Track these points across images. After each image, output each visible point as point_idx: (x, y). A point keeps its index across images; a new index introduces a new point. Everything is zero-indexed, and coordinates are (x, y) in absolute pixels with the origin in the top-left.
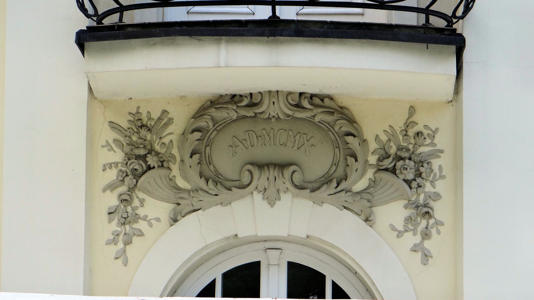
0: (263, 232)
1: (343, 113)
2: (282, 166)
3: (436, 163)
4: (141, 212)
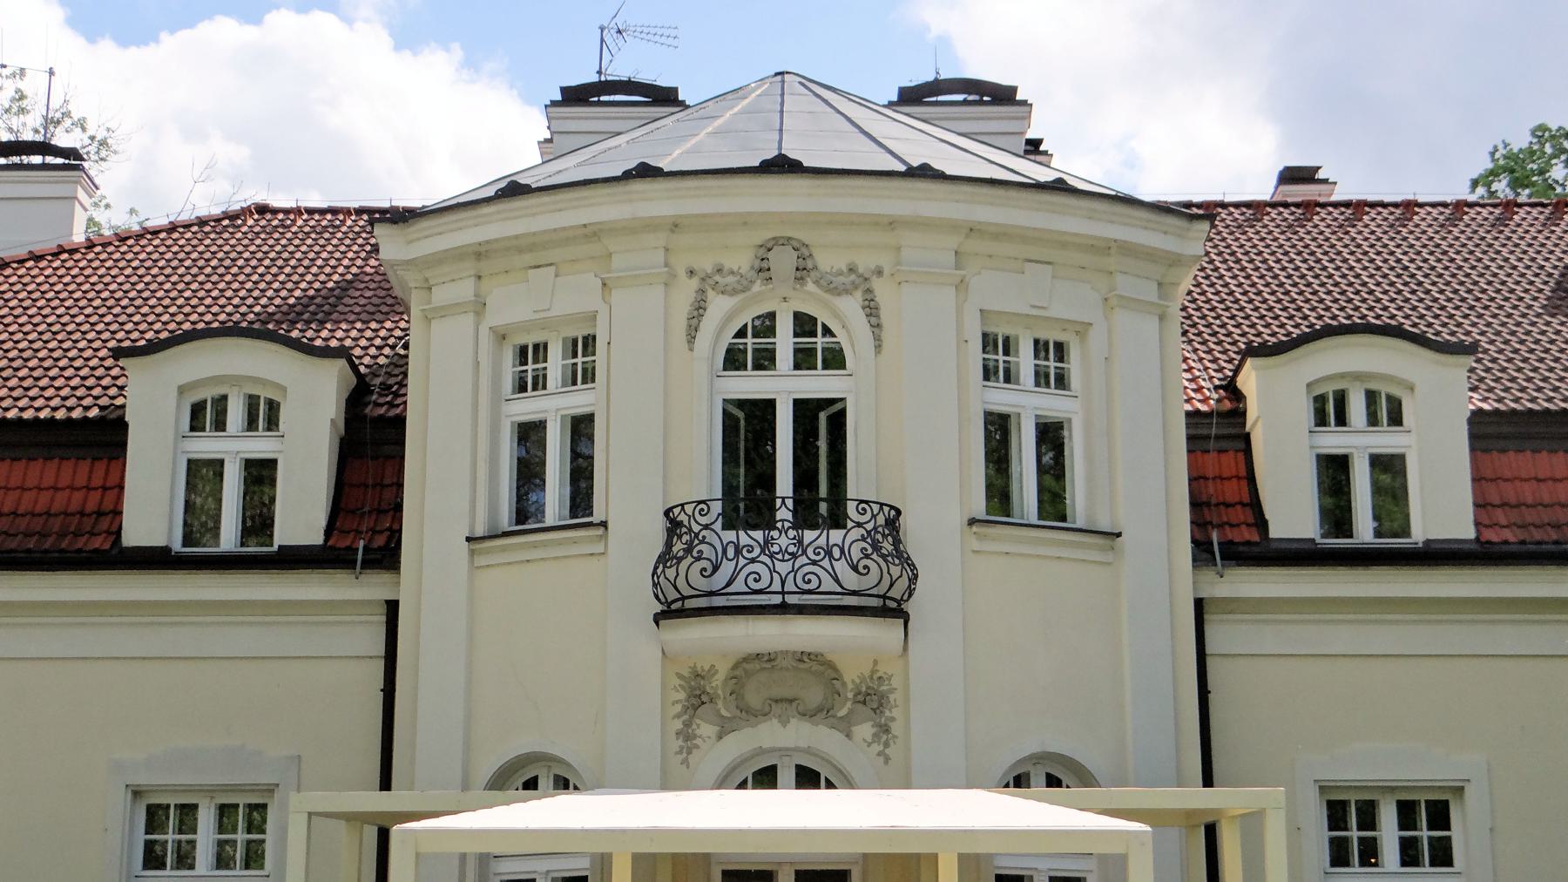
0: (780, 745)
1: (831, 666)
2: (791, 701)
3: (892, 697)
4: (698, 732)
